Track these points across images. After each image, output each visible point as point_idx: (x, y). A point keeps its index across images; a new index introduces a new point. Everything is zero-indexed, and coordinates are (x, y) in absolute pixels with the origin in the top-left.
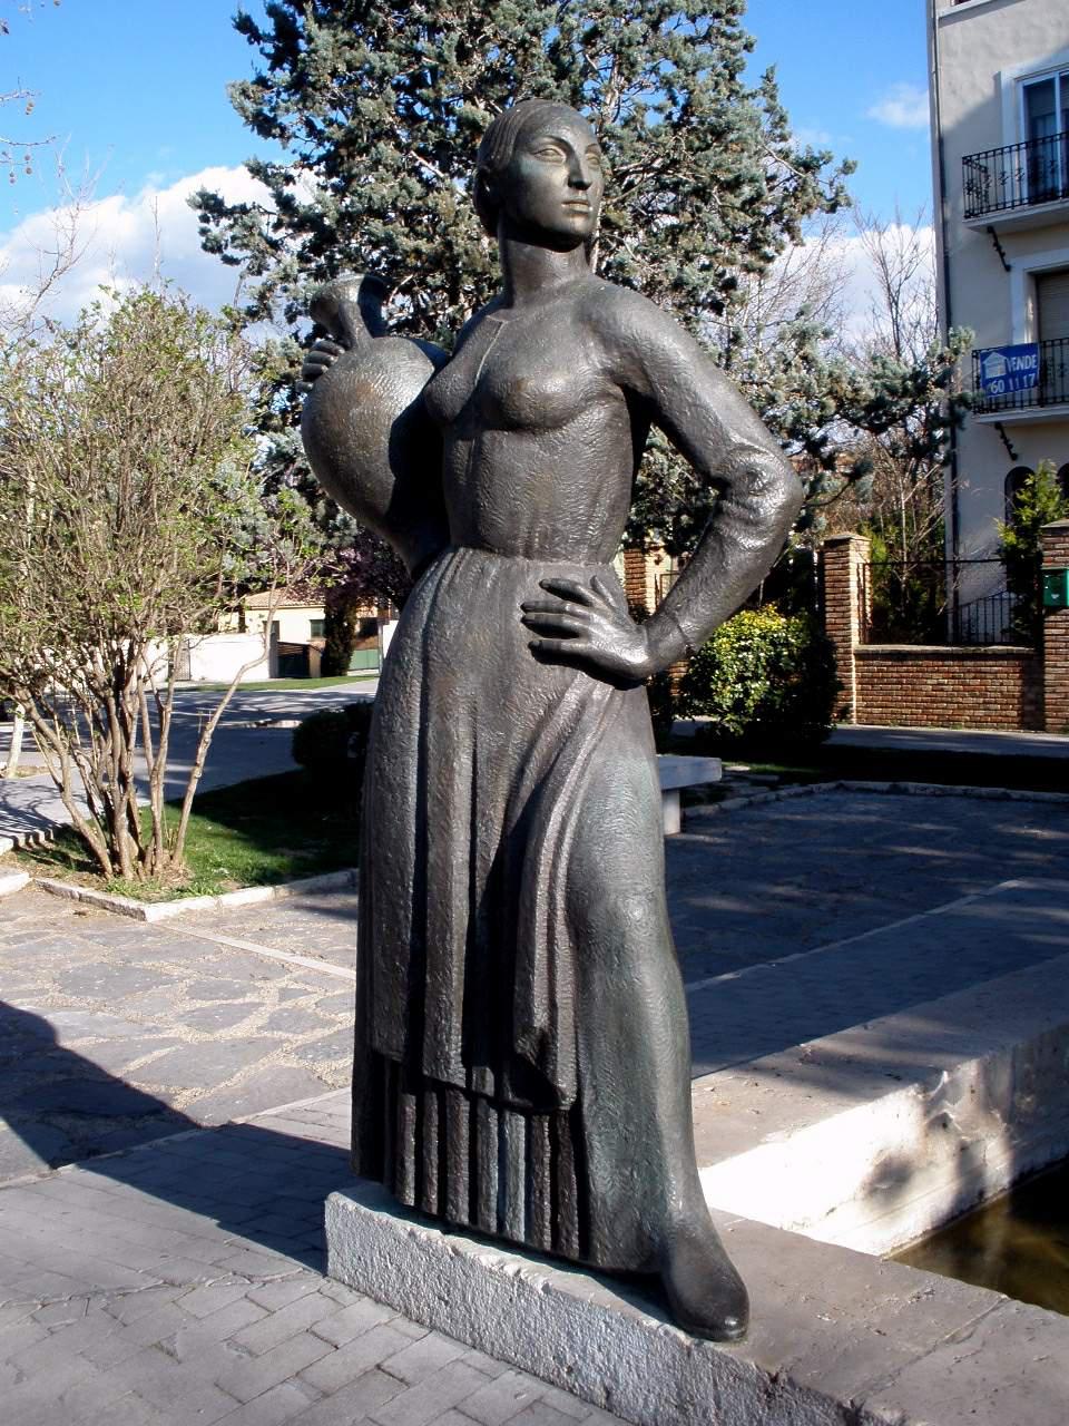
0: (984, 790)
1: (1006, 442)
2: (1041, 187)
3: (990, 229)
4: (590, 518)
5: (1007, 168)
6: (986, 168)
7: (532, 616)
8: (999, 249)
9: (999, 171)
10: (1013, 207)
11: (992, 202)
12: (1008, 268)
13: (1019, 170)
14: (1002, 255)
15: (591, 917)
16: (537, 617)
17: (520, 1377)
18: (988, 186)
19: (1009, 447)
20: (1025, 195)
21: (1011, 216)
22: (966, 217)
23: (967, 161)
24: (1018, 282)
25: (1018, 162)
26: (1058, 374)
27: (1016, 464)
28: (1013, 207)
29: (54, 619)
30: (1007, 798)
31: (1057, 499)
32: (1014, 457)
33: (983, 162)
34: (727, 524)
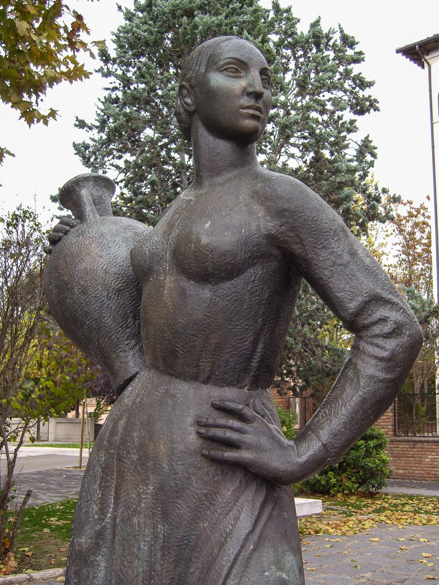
7: (203, 430)
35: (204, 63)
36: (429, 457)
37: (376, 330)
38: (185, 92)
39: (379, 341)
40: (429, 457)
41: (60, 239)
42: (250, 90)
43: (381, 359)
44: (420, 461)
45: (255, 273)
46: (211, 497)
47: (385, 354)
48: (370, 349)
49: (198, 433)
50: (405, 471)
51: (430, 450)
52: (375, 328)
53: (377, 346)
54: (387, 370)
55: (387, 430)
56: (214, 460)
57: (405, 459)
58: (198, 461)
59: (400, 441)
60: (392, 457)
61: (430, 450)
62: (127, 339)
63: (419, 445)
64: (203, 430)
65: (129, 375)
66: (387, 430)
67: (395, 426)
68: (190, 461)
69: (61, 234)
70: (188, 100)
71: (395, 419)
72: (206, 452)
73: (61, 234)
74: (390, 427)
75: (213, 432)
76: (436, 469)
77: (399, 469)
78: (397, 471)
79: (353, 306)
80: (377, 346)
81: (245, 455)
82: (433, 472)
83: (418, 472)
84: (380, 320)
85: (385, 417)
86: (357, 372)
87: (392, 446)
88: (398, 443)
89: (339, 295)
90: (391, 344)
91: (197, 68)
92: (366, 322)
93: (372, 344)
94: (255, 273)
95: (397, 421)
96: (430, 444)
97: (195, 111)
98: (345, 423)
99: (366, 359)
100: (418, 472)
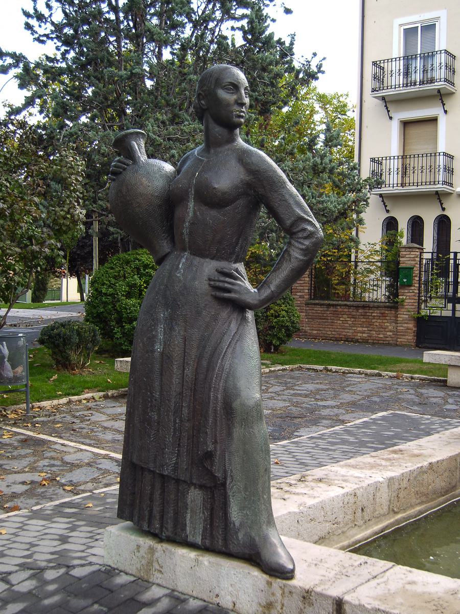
0: (369, 371)
1: (384, 204)
2: (409, 79)
3: (383, 98)
4: (237, 244)
5: (394, 69)
6: (383, 68)
7: (212, 283)
8: (387, 108)
9: (390, 69)
10: (395, 88)
11: (385, 85)
12: (391, 118)
13: (399, 70)
14: (388, 111)
15: (234, 405)
16: (215, 284)
17: (195, 601)
18: (384, 77)
19: (386, 206)
20: (401, 83)
21: (395, 93)
22: (372, 91)
23: (374, 63)
24: (395, 128)
25: (395, 165)
26: (412, 172)
27: (388, 215)
28: (395, 88)
29: (103, 276)
30: (380, 375)
31: (198, 482)
32: (388, 211)
33: (382, 65)
34: (293, 250)
35: (213, 82)
36: (341, 319)
37: (300, 235)
38: (201, 97)
39: (302, 241)
40: (341, 319)
41: (121, 173)
42: (239, 102)
43: (302, 249)
44: (332, 322)
45: (241, 202)
46: (215, 319)
47: (304, 247)
48: (296, 244)
49: (210, 285)
50: (319, 332)
51: (342, 313)
52: (299, 234)
53: (300, 243)
54: (305, 255)
55: (303, 294)
56: (216, 298)
57: (318, 320)
58: (209, 298)
59: (315, 304)
60: (307, 318)
61: (342, 313)
62: (163, 233)
63: (331, 309)
64: (212, 283)
65: (165, 253)
66: (303, 294)
67: (311, 290)
68: (206, 298)
69: (121, 170)
70: (203, 102)
71: (311, 284)
72: (213, 293)
73: (121, 170)
74: (307, 291)
75: (218, 284)
76: (346, 331)
77: (313, 330)
78: (311, 332)
79: (288, 222)
80: (300, 243)
81: (232, 295)
82: (344, 333)
83: (329, 333)
84: (302, 230)
85: (302, 282)
86: (290, 255)
87: (308, 308)
88: (313, 306)
89: (282, 216)
90: (307, 242)
91: (209, 85)
92: (295, 231)
93: (297, 242)
94: (241, 202)
95: (313, 286)
96: (342, 307)
97: (206, 109)
98: (283, 281)
99: (295, 249)
100: (329, 333)
